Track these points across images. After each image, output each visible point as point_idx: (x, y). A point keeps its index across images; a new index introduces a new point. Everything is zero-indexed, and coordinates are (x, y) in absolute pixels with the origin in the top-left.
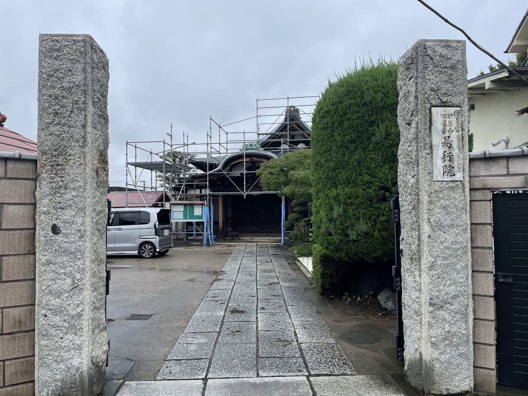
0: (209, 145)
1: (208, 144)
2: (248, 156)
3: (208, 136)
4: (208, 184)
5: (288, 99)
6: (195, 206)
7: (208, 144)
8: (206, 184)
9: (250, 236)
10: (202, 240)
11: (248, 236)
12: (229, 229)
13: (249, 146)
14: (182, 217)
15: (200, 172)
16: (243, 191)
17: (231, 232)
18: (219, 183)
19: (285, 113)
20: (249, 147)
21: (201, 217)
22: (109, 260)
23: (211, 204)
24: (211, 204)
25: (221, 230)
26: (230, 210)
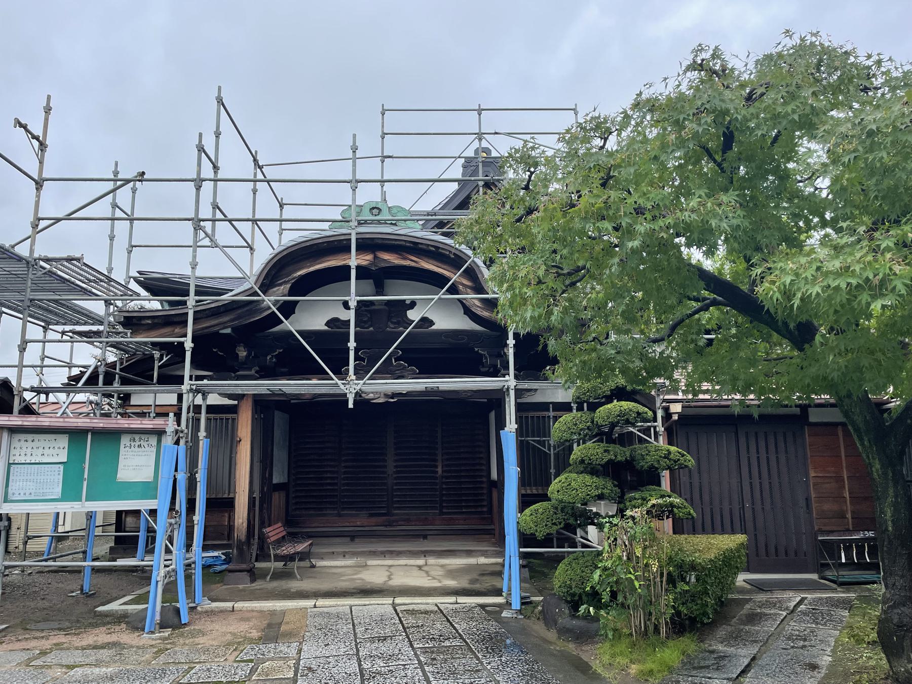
0: (207, 187)
1: (198, 183)
2: (366, 245)
3: (201, 149)
4: (189, 345)
5: (480, 111)
6: (125, 440)
7: (198, 183)
8: (181, 344)
9: (354, 554)
10: (197, 293)
11: (344, 555)
12: (274, 532)
13: (366, 211)
14: (58, 491)
15: (154, 305)
16: (340, 371)
17: (280, 542)
18: (242, 353)
19: (457, 172)
20: (366, 216)
21: (148, 489)
22: (498, 568)
23: (202, 434)
24: (202, 434)
25: (243, 537)
26: (280, 456)
